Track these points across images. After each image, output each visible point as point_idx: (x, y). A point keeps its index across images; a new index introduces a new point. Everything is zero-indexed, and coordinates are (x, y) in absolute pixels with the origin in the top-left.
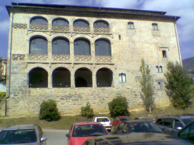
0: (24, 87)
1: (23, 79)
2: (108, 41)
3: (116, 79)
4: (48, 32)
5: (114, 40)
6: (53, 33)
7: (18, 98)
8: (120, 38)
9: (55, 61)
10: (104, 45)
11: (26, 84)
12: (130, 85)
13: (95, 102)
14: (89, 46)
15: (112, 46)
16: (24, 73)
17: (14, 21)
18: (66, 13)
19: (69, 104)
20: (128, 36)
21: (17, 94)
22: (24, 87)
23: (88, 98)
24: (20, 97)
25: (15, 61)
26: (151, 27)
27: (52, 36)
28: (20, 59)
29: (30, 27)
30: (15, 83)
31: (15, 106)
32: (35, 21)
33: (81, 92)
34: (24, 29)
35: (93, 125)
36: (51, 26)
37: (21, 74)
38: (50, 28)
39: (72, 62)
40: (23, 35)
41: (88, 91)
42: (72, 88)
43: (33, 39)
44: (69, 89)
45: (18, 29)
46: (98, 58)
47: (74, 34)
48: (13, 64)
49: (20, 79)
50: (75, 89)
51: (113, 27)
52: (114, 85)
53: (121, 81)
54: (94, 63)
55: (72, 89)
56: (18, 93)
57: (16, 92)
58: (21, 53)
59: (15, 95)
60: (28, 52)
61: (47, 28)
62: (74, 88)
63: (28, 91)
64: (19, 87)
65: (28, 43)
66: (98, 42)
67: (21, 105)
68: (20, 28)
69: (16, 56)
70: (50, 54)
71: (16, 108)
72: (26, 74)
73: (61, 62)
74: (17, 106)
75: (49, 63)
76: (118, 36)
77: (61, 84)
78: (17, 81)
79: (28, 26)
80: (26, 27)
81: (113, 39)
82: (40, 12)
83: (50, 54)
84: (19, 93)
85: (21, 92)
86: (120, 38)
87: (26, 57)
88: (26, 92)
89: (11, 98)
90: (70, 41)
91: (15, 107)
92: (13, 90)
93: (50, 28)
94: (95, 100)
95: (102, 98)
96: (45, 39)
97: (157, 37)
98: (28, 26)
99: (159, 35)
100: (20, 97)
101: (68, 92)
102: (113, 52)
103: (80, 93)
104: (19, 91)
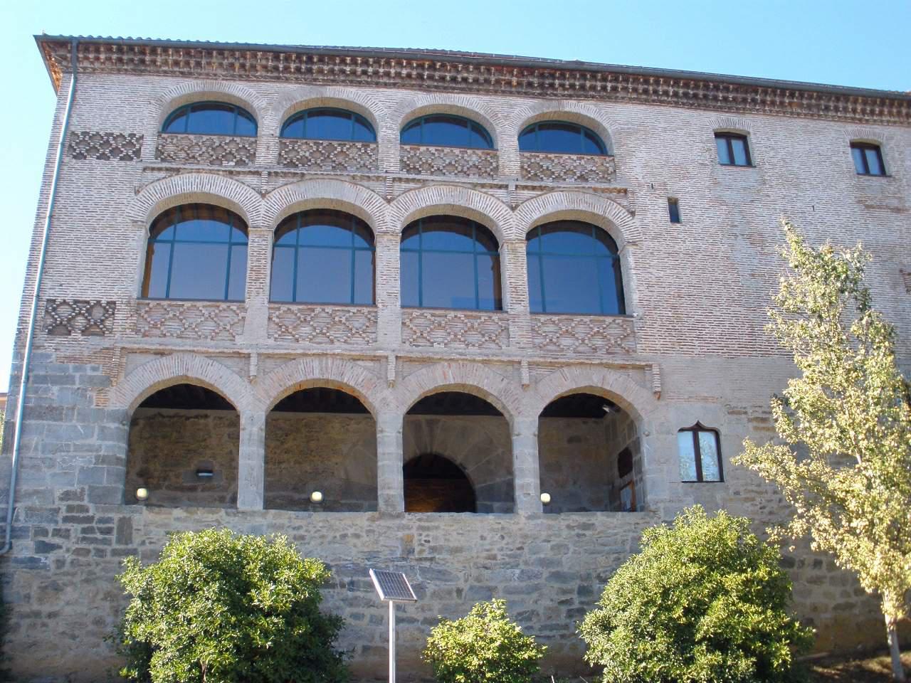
0: (99, 496)
1: (90, 449)
2: (603, 237)
3: (665, 456)
4: (257, 173)
5: (638, 228)
6: (281, 181)
7: (60, 563)
8: (675, 217)
9: (287, 347)
10: (583, 257)
11: (111, 480)
12: (746, 500)
13: (529, 606)
14: (487, 261)
15: (630, 260)
16: (100, 414)
17: (74, 120)
18: (364, 73)
19: (366, 620)
20: (723, 203)
21: (50, 539)
22: (99, 496)
23: (735, 416)
24: (69, 557)
25: (58, 339)
26: (849, 159)
27: (274, 196)
28: (84, 332)
29: (159, 153)
30: (47, 472)
31: (37, 614)
32: (535, 435)
33: (442, 542)
34: (123, 163)
35: (736, 84)
36: (274, 143)
37: (83, 417)
38: (267, 150)
39: (391, 353)
40: (116, 195)
41: (489, 536)
42: (383, 516)
43: (164, 221)
44: (359, 521)
45: (92, 160)
46: (552, 328)
47: (404, 185)
48: (49, 356)
49: (77, 448)
50: (404, 522)
51: (631, 154)
52: (649, 497)
53: (692, 475)
54: (520, 361)
55: (382, 523)
56: (57, 532)
57: (51, 527)
58: (90, 296)
59: (45, 548)
60: (134, 290)
61: (252, 157)
62: (399, 516)
63: (114, 525)
64: (66, 496)
65: (139, 238)
66: (546, 238)
67: (791, 466)
68: (102, 157)
69: (64, 311)
70: (257, 300)
71: (44, 625)
72: (113, 416)
73: (324, 353)
74: (52, 615)
75: (251, 352)
76: (663, 203)
77: (317, 496)
78: (58, 457)
79: (148, 149)
80: (137, 153)
81: (636, 222)
82: (220, 72)
83: (257, 300)
84: (66, 534)
85: (75, 529)
86: (675, 217)
87: (122, 317)
88: (109, 531)
89: (17, 561)
90: (377, 228)
91: (39, 621)
92: (31, 511)
93: (267, 150)
94: (535, 596)
95: (574, 585)
96: (235, 220)
97: (884, 214)
98: (148, 149)
99: (895, 203)
100: (69, 557)
101: (357, 536)
102: (635, 294)
103: (433, 549)
104: (66, 520)
